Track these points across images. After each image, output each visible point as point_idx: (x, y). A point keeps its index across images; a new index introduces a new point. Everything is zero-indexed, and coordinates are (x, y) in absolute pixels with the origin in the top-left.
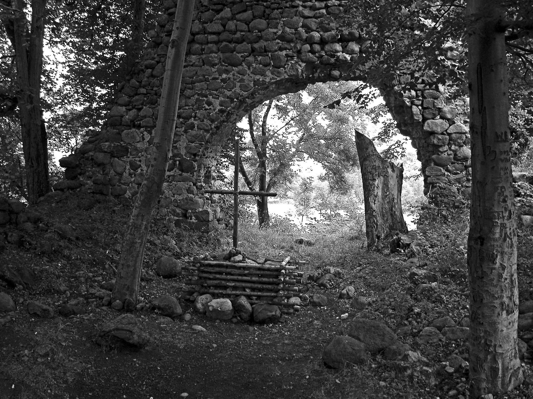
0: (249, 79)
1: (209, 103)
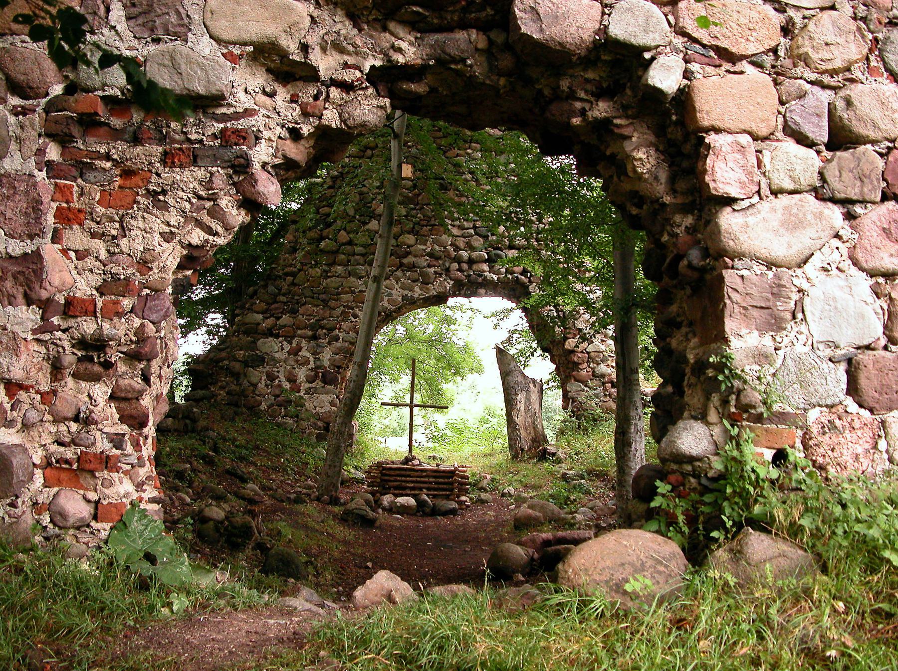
0: (397, 294)
1: (355, 316)
